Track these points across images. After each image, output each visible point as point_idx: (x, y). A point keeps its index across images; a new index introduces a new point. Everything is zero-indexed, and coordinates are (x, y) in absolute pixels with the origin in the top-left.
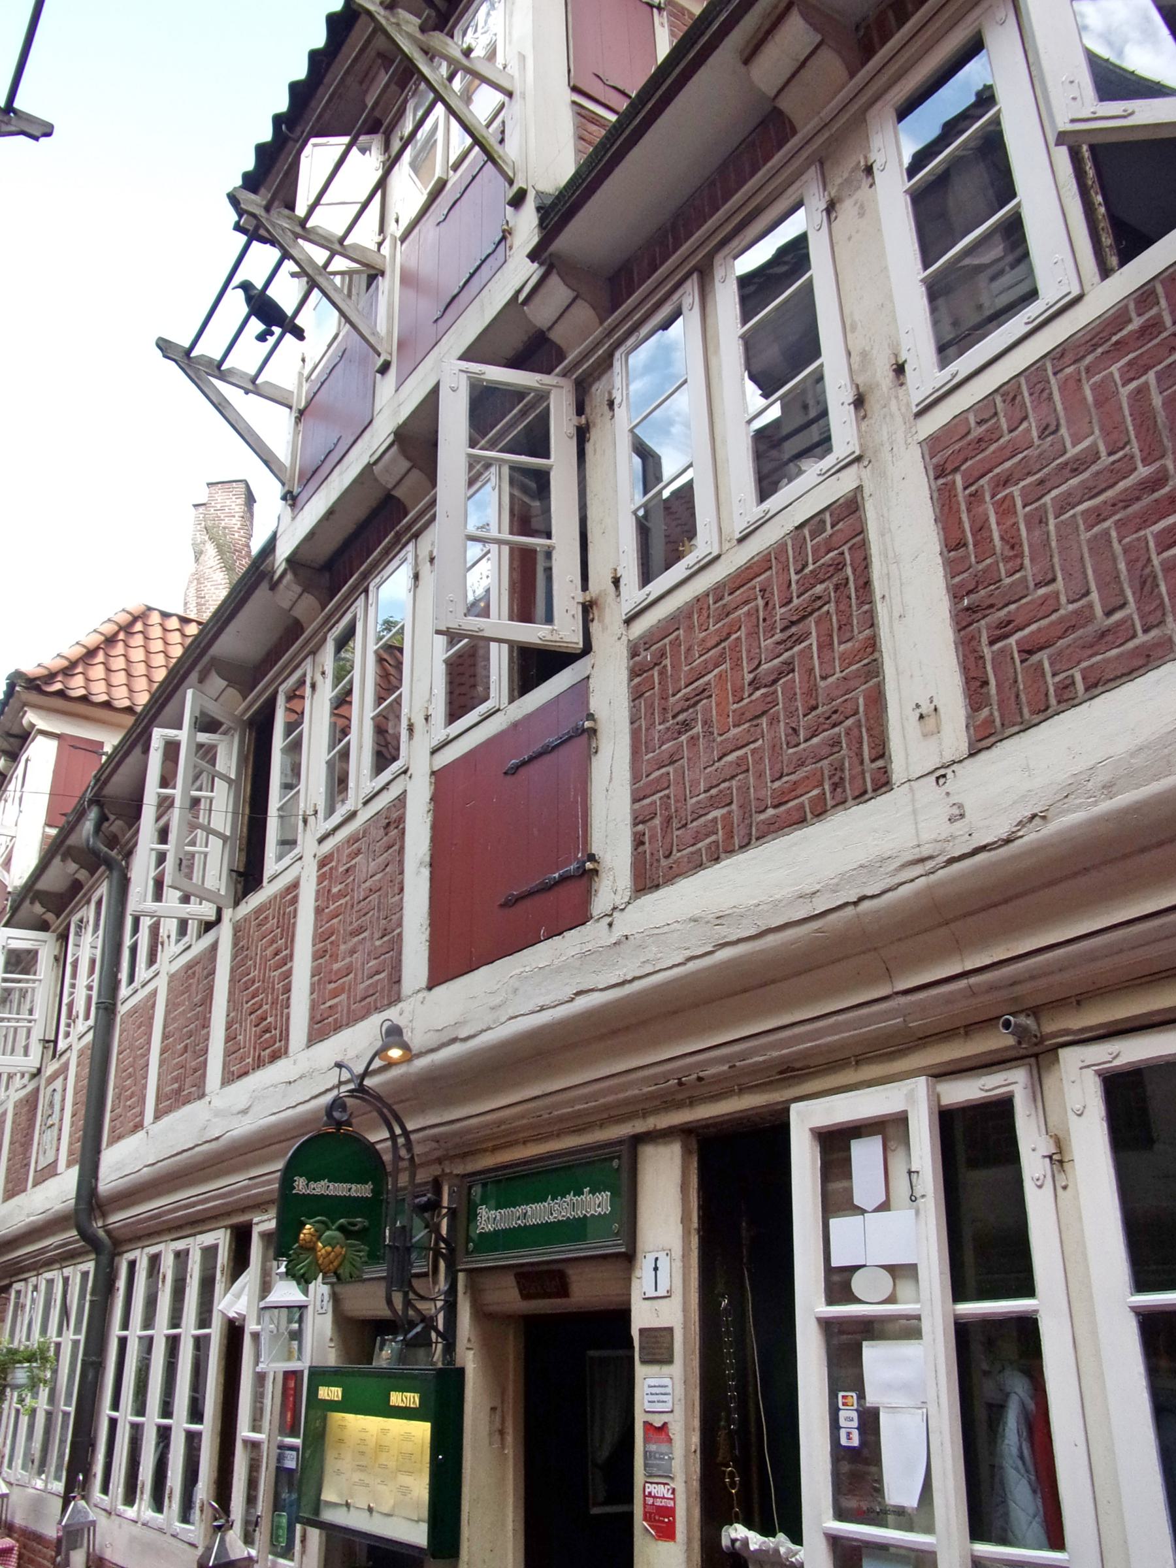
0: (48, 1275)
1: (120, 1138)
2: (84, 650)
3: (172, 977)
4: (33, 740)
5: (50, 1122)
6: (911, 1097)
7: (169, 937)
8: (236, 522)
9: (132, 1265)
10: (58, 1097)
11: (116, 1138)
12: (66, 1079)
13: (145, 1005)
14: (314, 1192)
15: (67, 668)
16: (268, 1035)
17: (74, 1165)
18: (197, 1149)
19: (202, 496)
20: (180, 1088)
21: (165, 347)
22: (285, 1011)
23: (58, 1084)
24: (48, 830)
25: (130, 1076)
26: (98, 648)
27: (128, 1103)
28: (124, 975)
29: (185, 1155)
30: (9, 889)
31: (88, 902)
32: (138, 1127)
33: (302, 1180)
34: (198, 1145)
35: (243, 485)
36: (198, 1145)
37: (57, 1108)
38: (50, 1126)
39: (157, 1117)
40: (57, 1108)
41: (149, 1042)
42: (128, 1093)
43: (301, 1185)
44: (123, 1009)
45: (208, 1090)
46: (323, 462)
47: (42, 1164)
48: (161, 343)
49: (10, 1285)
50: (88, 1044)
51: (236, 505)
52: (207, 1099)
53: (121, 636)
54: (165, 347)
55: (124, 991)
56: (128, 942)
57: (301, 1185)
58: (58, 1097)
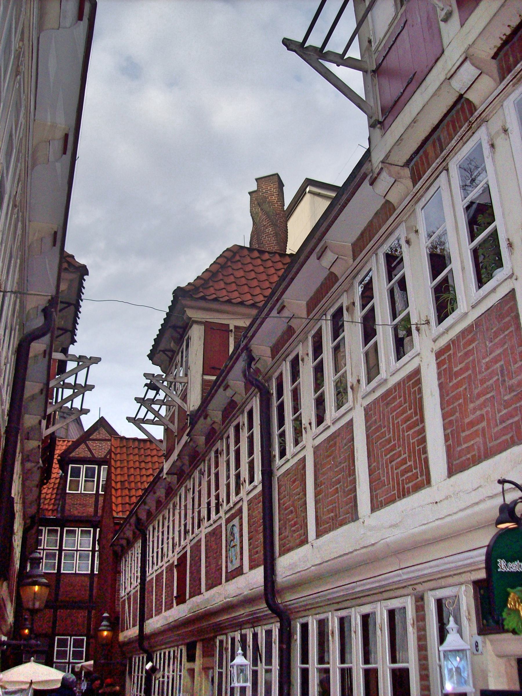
0: (232, 634)
1: (289, 550)
2: (211, 274)
3: (167, 568)
4: (191, 327)
5: (232, 544)
6: (406, 602)
7: (310, 424)
8: (274, 198)
9: (305, 627)
10: (236, 530)
11: (286, 550)
12: (241, 518)
13: (297, 468)
14: (512, 570)
15: (203, 284)
16: (410, 474)
17: (258, 566)
18: (355, 553)
19: (254, 187)
20: (336, 516)
21: (287, 43)
22: (423, 456)
23: (236, 521)
24: (207, 377)
25: (291, 512)
26: (218, 272)
27: (293, 528)
28: (276, 452)
29: (345, 557)
30: (188, 413)
31: (243, 412)
32: (304, 541)
33: (502, 562)
34: (356, 550)
35: (276, 177)
36: (356, 550)
37: (237, 536)
38: (234, 546)
39: (318, 535)
40: (237, 536)
41: (304, 490)
42: (293, 522)
43: (502, 565)
44: (279, 473)
45: (360, 515)
46: (402, 94)
47: (231, 568)
48: (285, 40)
49: (215, 637)
50: (258, 494)
51: (273, 188)
52: (361, 520)
53: (229, 264)
54: (287, 43)
55: (278, 462)
56: (276, 432)
57: (502, 565)
58: (236, 530)
